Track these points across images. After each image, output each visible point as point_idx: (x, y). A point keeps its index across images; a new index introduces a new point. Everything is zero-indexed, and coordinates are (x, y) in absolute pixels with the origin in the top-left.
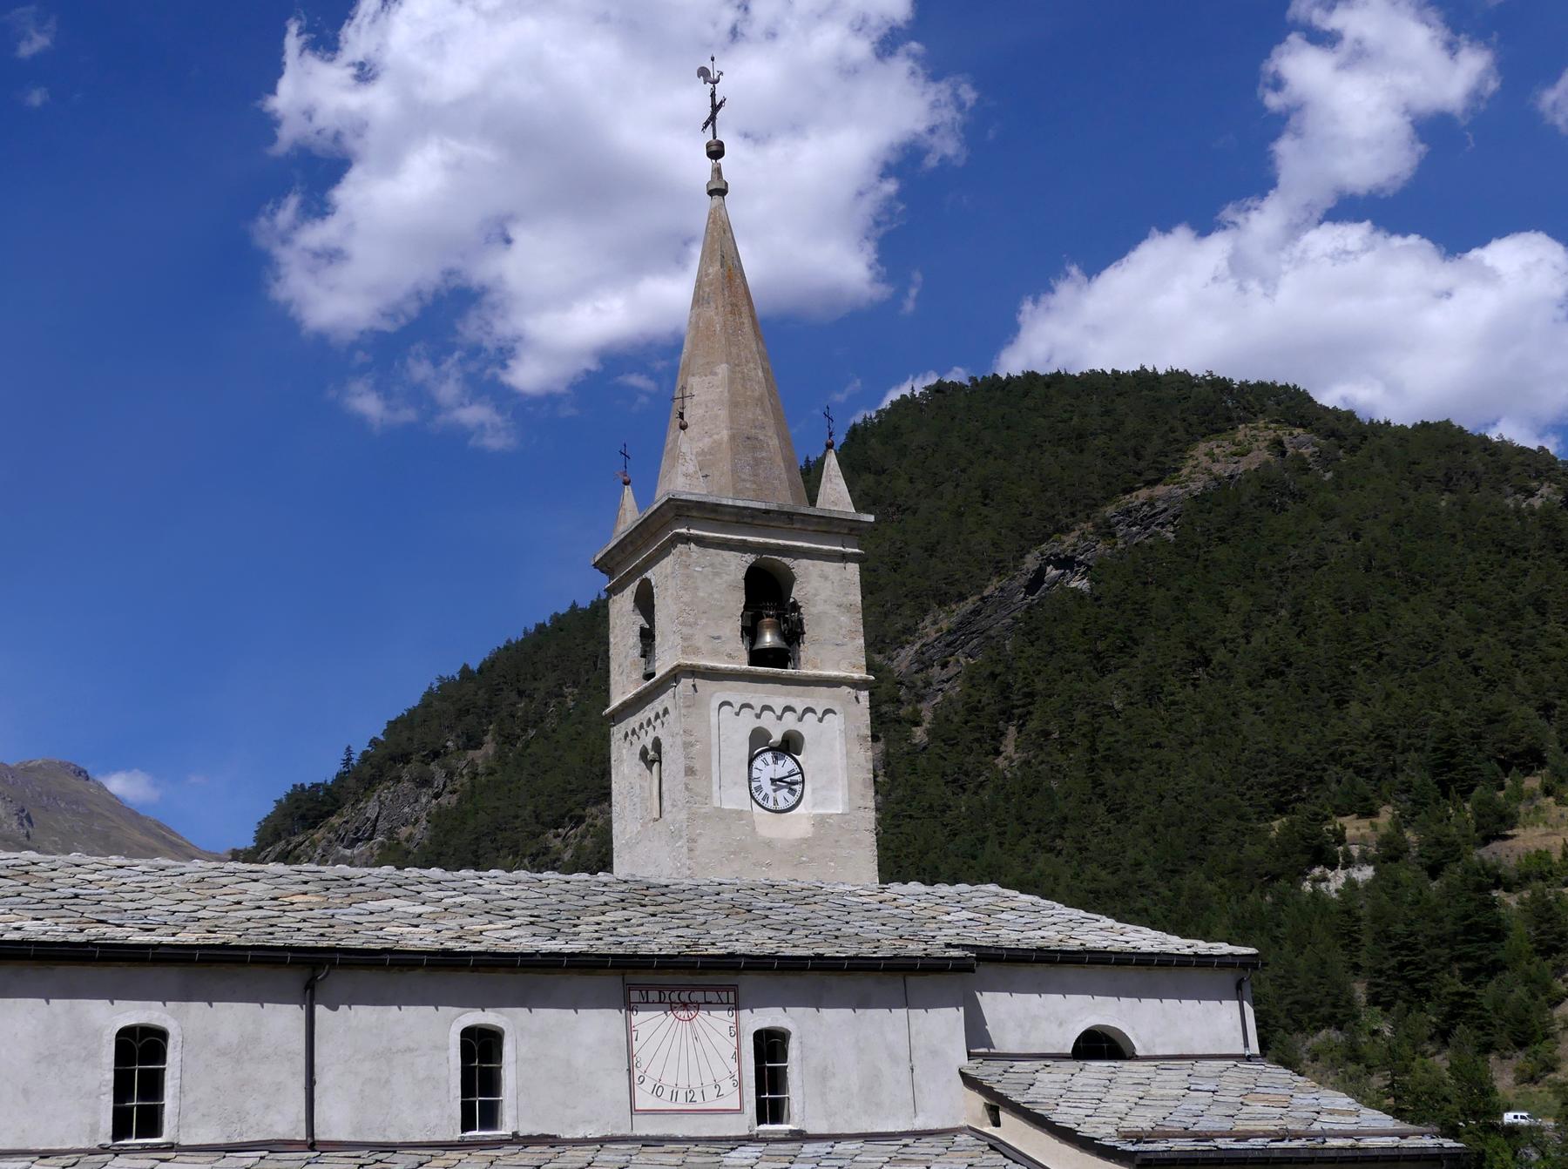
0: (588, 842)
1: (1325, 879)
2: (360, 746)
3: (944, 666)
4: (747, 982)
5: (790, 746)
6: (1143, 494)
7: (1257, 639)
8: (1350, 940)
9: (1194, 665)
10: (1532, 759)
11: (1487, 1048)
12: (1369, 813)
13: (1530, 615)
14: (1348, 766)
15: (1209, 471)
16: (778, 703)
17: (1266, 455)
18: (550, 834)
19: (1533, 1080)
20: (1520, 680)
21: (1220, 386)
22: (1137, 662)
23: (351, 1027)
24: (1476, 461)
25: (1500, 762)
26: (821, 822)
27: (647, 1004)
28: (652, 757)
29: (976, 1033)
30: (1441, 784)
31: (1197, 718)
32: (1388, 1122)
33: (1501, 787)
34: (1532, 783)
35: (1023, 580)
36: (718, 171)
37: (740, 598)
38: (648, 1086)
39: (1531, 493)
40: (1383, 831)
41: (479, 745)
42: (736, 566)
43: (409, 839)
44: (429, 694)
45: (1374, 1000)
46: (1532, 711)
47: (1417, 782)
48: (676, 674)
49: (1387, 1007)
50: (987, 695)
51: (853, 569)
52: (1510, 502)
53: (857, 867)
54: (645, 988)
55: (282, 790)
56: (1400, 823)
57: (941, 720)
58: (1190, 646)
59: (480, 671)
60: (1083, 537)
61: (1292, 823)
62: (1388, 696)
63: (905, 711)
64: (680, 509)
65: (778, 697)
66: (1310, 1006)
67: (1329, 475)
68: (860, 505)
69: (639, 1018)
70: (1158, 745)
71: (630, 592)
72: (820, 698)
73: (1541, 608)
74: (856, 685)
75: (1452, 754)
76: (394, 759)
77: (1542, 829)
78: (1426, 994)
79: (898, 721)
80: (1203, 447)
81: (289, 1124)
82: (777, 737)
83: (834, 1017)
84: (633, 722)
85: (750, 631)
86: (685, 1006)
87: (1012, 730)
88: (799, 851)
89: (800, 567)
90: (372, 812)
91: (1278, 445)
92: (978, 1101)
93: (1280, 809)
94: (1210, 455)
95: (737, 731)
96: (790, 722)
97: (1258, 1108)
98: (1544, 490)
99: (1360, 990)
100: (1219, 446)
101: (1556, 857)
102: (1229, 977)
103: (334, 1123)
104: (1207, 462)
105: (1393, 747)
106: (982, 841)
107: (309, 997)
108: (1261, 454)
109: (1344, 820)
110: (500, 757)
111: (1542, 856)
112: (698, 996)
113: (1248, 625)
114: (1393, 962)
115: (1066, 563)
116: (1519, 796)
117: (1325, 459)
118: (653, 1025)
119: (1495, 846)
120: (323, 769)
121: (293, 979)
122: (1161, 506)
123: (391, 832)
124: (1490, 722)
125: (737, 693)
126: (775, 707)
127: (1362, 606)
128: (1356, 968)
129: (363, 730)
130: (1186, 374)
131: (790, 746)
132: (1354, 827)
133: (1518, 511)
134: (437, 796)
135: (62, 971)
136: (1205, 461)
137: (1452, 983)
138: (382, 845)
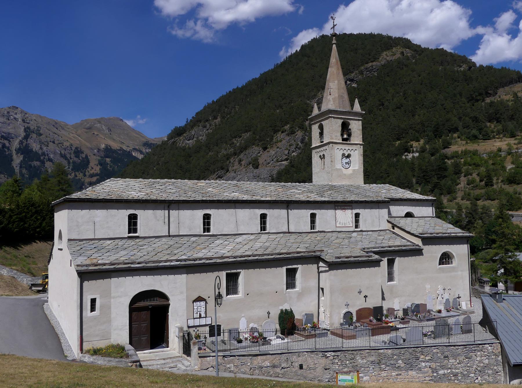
0: (243, 142)
1: (408, 155)
2: (190, 118)
4: (354, 205)
5: (349, 156)
6: (370, 64)
7: (395, 100)
8: (413, 170)
9: (380, 105)
10: (456, 130)
11: (441, 194)
12: (418, 141)
13: (458, 96)
14: (414, 130)
15: (386, 59)
16: (347, 148)
17: (399, 55)
18: (234, 140)
19: (451, 201)
21: (390, 38)
23: (294, 213)
25: (449, 130)
26: (354, 170)
27: (338, 209)
28: (322, 157)
29: (389, 213)
30: (435, 135)
31: (380, 118)
33: (448, 136)
34: (455, 135)
37: (341, 128)
38: (338, 223)
39: (461, 67)
40: (421, 145)
41: (216, 119)
42: (340, 122)
43: (202, 139)
44: (205, 107)
45: (417, 183)
46: (457, 119)
47: (430, 134)
48: (329, 143)
49: (420, 185)
51: (361, 122)
52: (456, 69)
53: (360, 180)
54: (338, 206)
55: (173, 128)
56: (425, 144)
59: (216, 101)
60: (356, 74)
61: (401, 143)
62: (424, 114)
64: (330, 112)
65: (347, 147)
67: (414, 61)
68: (362, 110)
69: (337, 211)
70: (371, 124)
71: (317, 125)
72: (354, 147)
73: (461, 94)
74: (360, 145)
75: (438, 128)
76: (198, 121)
77: (457, 146)
78: (429, 182)
80: (385, 53)
81: (285, 229)
82: (346, 155)
83: (367, 211)
84: (318, 150)
85: (342, 135)
86: (344, 209)
88: (350, 177)
89: (351, 122)
90: (193, 133)
91: (402, 53)
92: (390, 225)
93: (398, 139)
94: (386, 55)
95: (339, 154)
96: (349, 152)
97: (437, 227)
98: (464, 66)
99: (414, 180)
100: (389, 53)
101: (460, 152)
102: (431, 203)
103: (292, 229)
104: (386, 57)
105: (424, 126)
107: (287, 208)
108: (398, 55)
109: (412, 142)
110: (222, 121)
111: (457, 152)
112: (346, 207)
114: (422, 175)
116: (452, 138)
117: (414, 57)
118: (339, 212)
119: (446, 149)
120: (182, 123)
122: (374, 67)
123: (197, 138)
124: (447, 121)
125: (340, 146)
126: (346, 149)
128: (414, 176)
129: (190, 115)
130: (382, 34)
131: (349, 156)
132: (415, 144)
133: (457, 71)
134: (207, 130)
135: (252, 205)
136: (385, 56)
137: (435, 180)
138: (196, 141)
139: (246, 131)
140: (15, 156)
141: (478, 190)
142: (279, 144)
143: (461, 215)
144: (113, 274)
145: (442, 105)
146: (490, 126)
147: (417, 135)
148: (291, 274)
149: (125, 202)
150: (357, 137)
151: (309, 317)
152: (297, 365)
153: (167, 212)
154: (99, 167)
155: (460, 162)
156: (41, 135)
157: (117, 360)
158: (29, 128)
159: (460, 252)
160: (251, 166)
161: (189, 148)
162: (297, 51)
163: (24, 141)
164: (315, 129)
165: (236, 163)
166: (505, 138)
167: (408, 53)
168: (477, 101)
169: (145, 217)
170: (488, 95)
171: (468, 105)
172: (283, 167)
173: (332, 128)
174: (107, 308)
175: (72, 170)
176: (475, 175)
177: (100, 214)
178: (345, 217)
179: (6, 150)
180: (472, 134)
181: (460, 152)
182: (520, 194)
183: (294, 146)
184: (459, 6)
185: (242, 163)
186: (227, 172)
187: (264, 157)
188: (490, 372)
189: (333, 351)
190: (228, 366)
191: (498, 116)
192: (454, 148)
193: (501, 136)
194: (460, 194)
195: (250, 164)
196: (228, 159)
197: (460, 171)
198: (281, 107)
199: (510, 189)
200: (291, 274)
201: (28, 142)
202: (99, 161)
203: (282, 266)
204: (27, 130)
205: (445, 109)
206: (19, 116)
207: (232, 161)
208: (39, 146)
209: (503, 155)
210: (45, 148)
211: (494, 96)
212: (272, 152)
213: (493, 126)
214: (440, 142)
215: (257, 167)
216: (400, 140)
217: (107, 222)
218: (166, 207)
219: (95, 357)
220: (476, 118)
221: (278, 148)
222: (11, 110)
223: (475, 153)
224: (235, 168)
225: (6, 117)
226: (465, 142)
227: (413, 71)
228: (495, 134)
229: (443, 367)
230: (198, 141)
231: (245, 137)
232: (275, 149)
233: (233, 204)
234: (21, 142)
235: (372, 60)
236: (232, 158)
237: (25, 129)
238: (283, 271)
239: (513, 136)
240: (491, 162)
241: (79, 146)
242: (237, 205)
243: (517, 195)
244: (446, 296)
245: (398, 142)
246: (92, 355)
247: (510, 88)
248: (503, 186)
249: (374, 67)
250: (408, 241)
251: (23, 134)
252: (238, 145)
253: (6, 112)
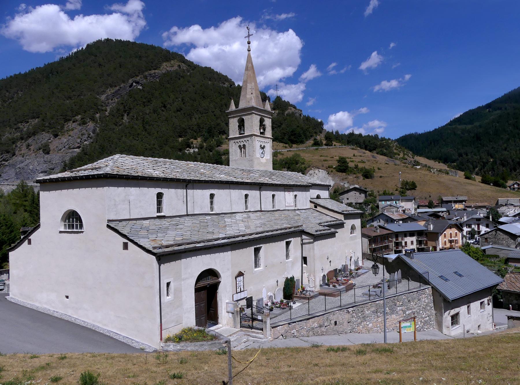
3: (112, 100)
6: (153, 71)
17: (177, 68)
20: (222, 118)
22: (152, 105)
26: (267, 160)
32: (353, 209)
35: (129, 85)
36: (249, 47)
50: (122, 107)
53: (270, 168)
57: (112, 111)
58: (162, 103)
61: (184, 140)
62: (199, 118)
67: (188, 74)
74: (271, 138)
79: (102, 110)
80: (165, 64)
87: (126, 115)
89: (265, 119)
91: (179, 66)
93: (181, 137)
94: (166, 65)
104: (166, 67)
106: (122, 136)
107: (260, 189)
108: (176, 68)
109: (192, 140)
119: (219, 147)
121: (258, 187)
122: (156, 74)
124: (217, 125)
127: (195, 100)
132: (195, 142)
136: (165, 67)
139: (34, 118)
142: (71, 133)
144: (183, 255)
145: (213, 112)
149: (49, 182)
152: (333, 322)
153: (185, 190)
157: (210, 343)
162: (82, 48)
164: (234, 123)
165: (24, 147)
167: (184, 67)
169: (171, 195)
172: (75, 154)
174: (178, 291)
177: (133, 192)
183: (86, 136)
184: (298, 38)
185: (30, 147)
186: (13, 156)
187: (55, 144)
188: (429, 308)
189: (352, 307)
190: (292, 332)
195: (40, 149)
196: (13, 143)
198: (70, 98)
203: (283, 240)
205: (215, 115)
207: (19, 146)
214: (213, 142)
215: (48, 153)
216: (181, 137)
217: (140, 201)
218: (185, 187)
219: (182, 344)
221: (70, 136)
224: (22, 152)
227: (189, 82)
229: (408, 309)
231: (33, 123)
232: (67, 136)
233: (228, 185)
235: (155, 68)
236: (19, 143)
238: (284, 243)
242: (231, 185)
246: (178, 342)
249: (156, 74)
250: (335, 218)
252: (25, 129)
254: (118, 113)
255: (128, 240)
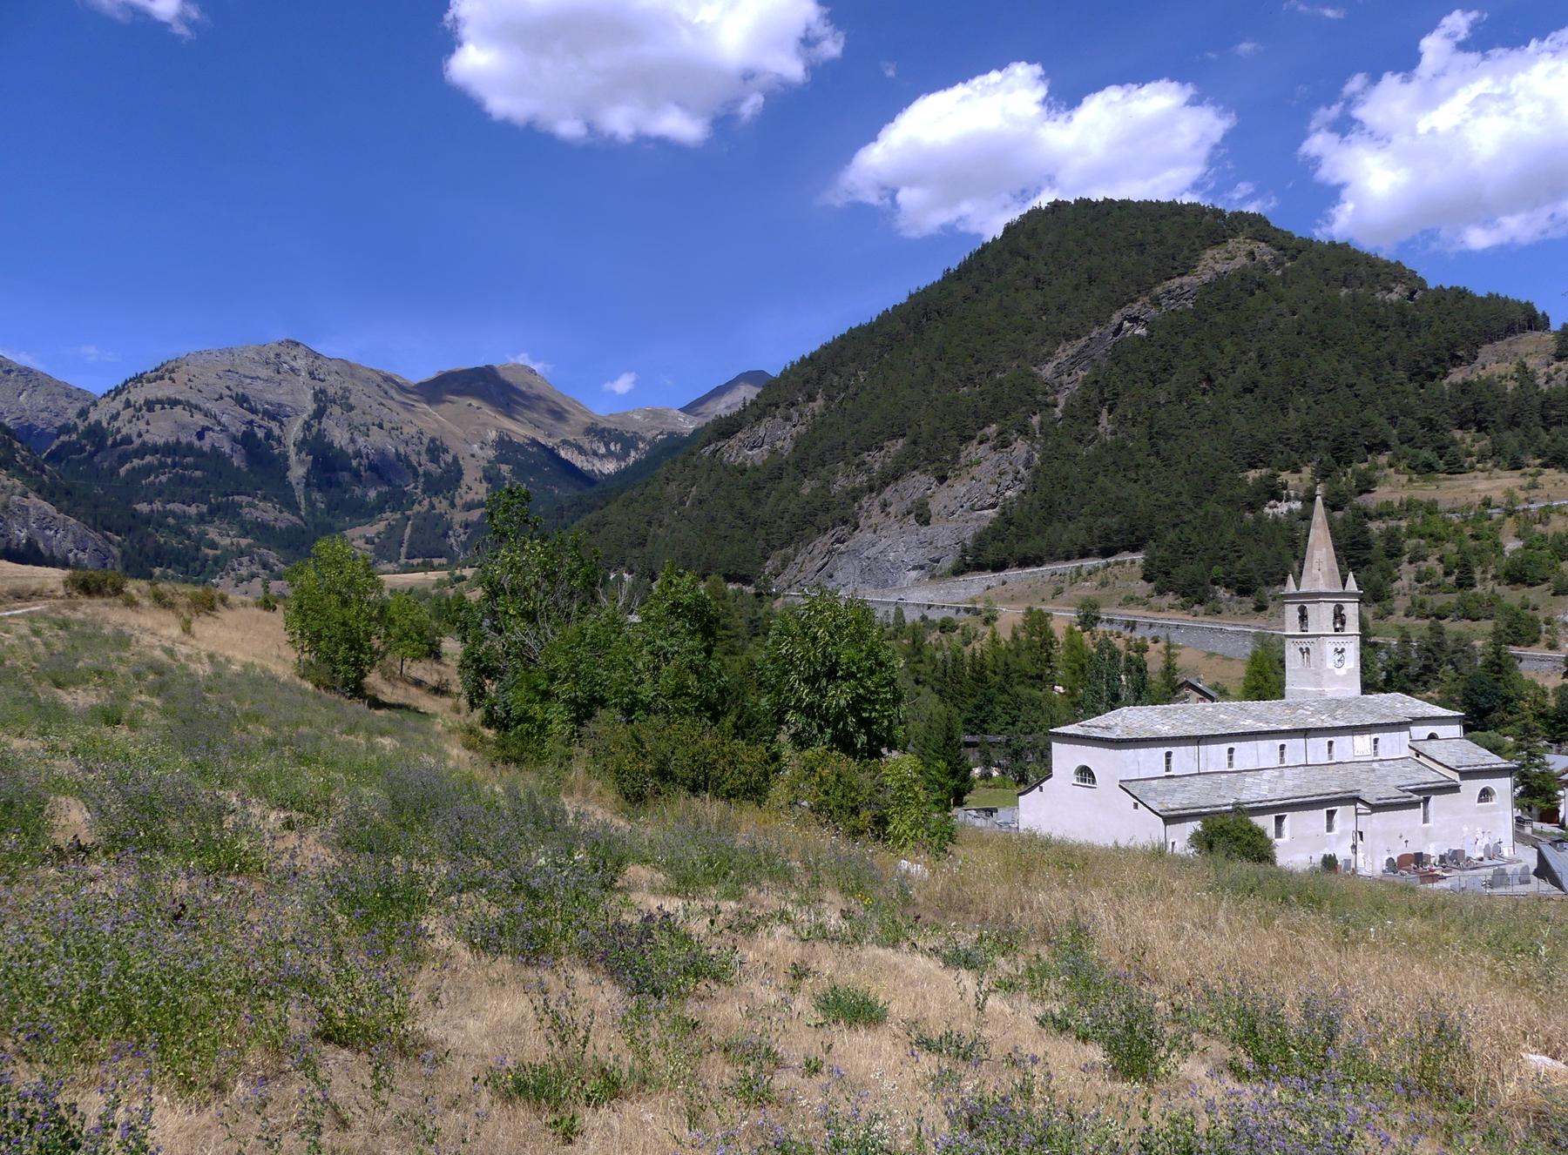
6: (1177, 281)
7: (1239, 370)
10: (1384, 446)
17: (1245, 260)
23: (1312, 741)
24: (1363, 270)
34: (1383, 459)
39: (1391, 290)
50: (1094, 394)
57: (1069, 405)
63: (1050, 399)
65: (1340, 640)
66: (1272, 575)
80: (1209, 253)
87: (1105, 411)
88: (1344, 679)
90: (762, 433)
91: (1251, 254)
104: (1213, 263)
108: (1242, 260)
113: (1234, 363)
115: (1134, 320)
118: (1357, 738)
119: (1365, 496)
122: (1186, 288)
126: (1339, 642)
139: (894, 436)
140: (293, 458)
141: (1440, 595)
142: (975, 471)
143: (1408, 653)
145: (1351, 386)
146: (1463, 439)
147: (1295, 456)
148: (1331, 814)
150: (1353, 627)
151: (1348, 862)
154: (485, 485)
155: (1398, 528)
156: (351, 408)
158: (323, 391)
159: (1503, 787)
160: (912, 519)
161: (756, 469)
163: (315, 423)
165: (876, 510)
166: (1496, 470)
167: (1265, 252)
168: (1432, 377)
170: (1456, 360)
171: (1411, 387)
172: (986, 524)
173: (1321, 615)
175: (424, 492)
176: (1432, 562)
178: (1363, 743)
179: (274, 443)
180: (1421, 459)
181: (1396, 504)
182: (1535, 609)
183: (1011, 476)
187: (941, 499)
191: (1480, 415)
192: (1382, 494)
193: (1489, 465)
194: (1401, 604)
196: (855, 499)
197: (1400, 550)
198: (970, 380)
199: (1512, 596)
200: (1331, 814)
201: (323, 425)
202: (484, 470)
204: (320, 395)
205: (1356, 396)
206: (300, 364)
208: (347, 436)
209: (1495, 517)
210: (361, 441)
211: (1469, 364)
212: (960, 488)
213: (1468, 440)
215: (926, 523)
220: (1431, 420)
222: (283, 349)
223: (1431, 508)
224: (873, 521)
225: (272, 367)
226: (1406, 477)
228: (1474, 459)
230: (774, 452)
234: (307, 426)
235: (1181, 270)
237: (315, 395)
239: (1516, 465)
240: (1468, 531)
241: (437, 435)
243: (1529, 612)
244: (1486, 840)
245: (1253, 474)
247: (1510, 344)
248: (1497, 588)
249: (1186, 288)
251: (311, 407)
253: (272, 356)
254: (1084, 412)
255: (1138, 801)
